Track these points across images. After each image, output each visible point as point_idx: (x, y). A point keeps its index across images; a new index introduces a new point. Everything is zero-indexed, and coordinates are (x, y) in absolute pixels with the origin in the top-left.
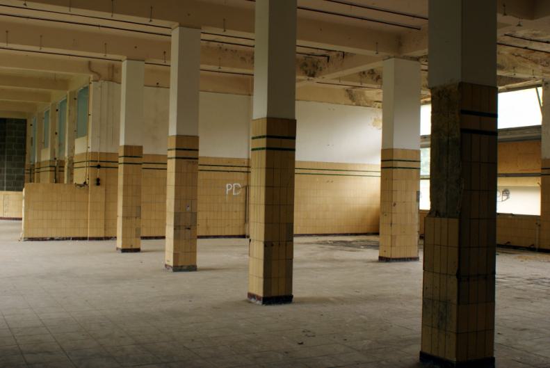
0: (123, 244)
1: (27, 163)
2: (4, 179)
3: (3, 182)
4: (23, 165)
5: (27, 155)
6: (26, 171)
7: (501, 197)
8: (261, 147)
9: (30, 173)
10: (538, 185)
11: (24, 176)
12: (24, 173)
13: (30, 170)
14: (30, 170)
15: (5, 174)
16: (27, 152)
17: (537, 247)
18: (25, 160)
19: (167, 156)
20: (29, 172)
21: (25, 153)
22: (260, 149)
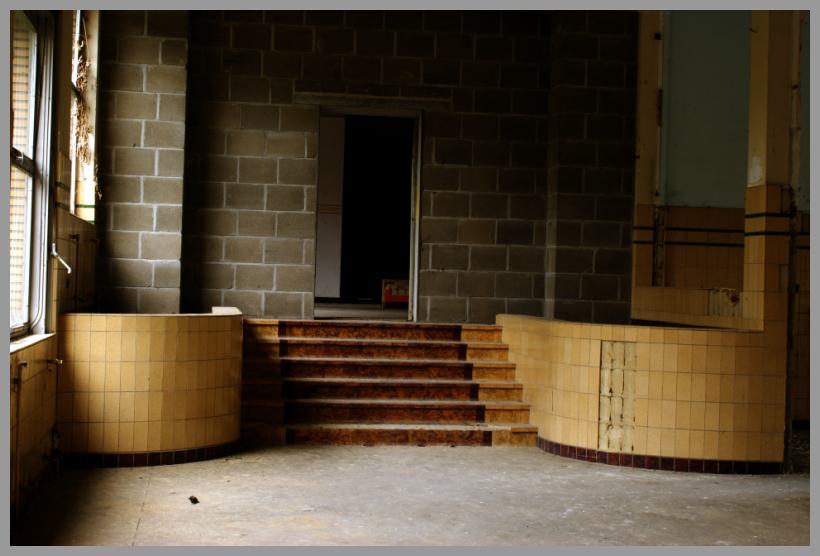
0: (174, 230)
1: (640, 196)
2: (541, 267)
3: (540, 280)
4: (625, 208)
5: (641, 169)
6: (635, 235)
7: (587, 381)
8: (758, 230)
9: (654, 242)
10: (224, 262)
11: (628, 255)
12: (627, 242)
13: (655, 229)
14: (655, 229)
15: (551, 247)
16: (641, 149)
17: (440, 351)
18: (630, 189)
19: (743, 210)
20: (648, 236)
21: (630, 157)
22: (757, 234)
